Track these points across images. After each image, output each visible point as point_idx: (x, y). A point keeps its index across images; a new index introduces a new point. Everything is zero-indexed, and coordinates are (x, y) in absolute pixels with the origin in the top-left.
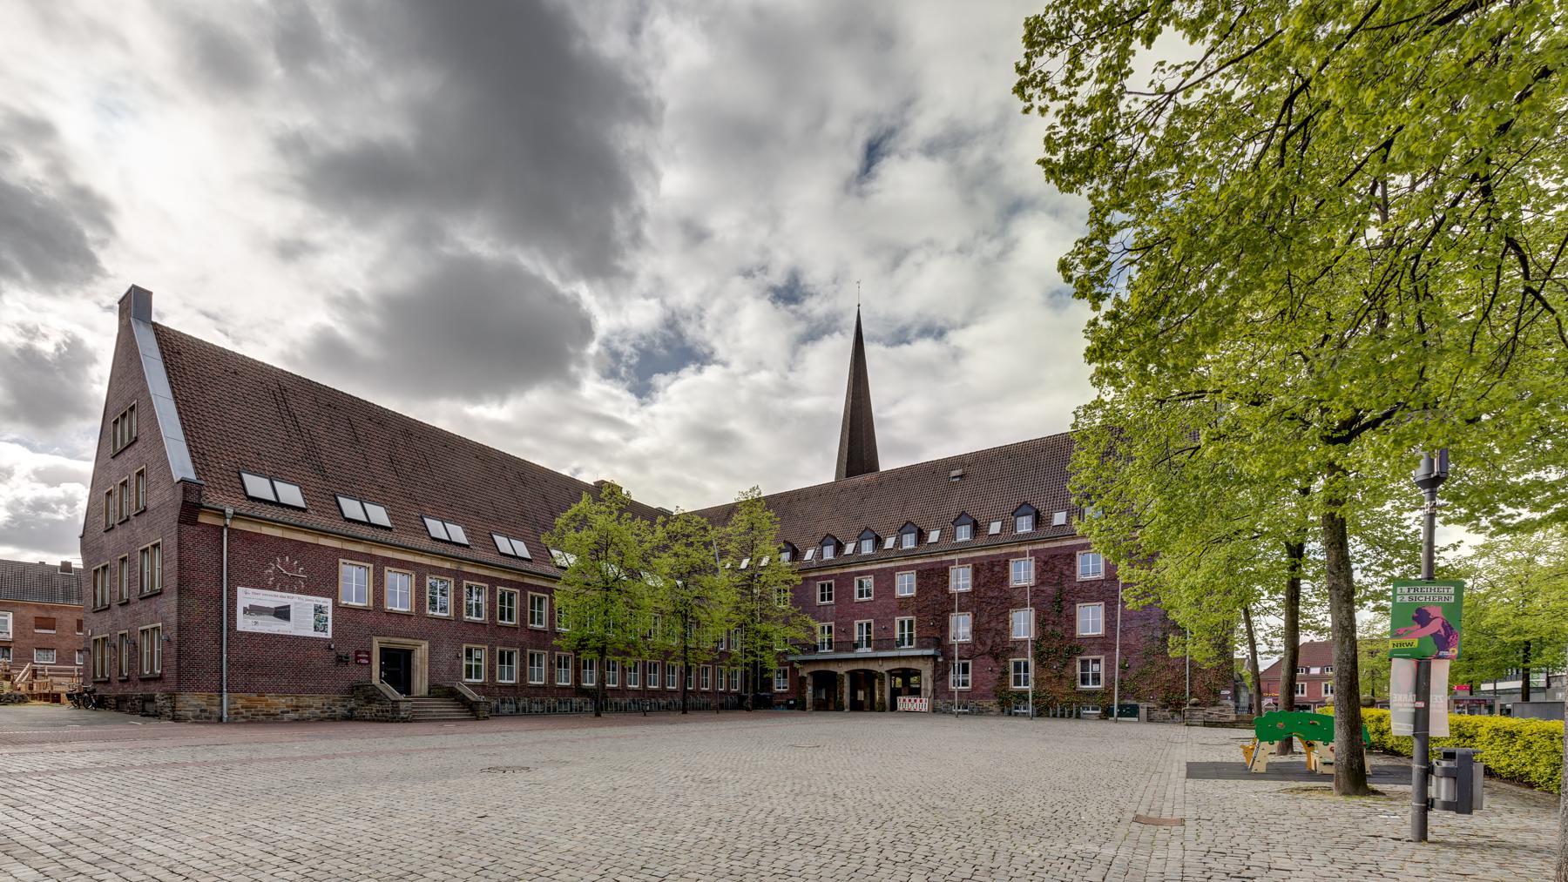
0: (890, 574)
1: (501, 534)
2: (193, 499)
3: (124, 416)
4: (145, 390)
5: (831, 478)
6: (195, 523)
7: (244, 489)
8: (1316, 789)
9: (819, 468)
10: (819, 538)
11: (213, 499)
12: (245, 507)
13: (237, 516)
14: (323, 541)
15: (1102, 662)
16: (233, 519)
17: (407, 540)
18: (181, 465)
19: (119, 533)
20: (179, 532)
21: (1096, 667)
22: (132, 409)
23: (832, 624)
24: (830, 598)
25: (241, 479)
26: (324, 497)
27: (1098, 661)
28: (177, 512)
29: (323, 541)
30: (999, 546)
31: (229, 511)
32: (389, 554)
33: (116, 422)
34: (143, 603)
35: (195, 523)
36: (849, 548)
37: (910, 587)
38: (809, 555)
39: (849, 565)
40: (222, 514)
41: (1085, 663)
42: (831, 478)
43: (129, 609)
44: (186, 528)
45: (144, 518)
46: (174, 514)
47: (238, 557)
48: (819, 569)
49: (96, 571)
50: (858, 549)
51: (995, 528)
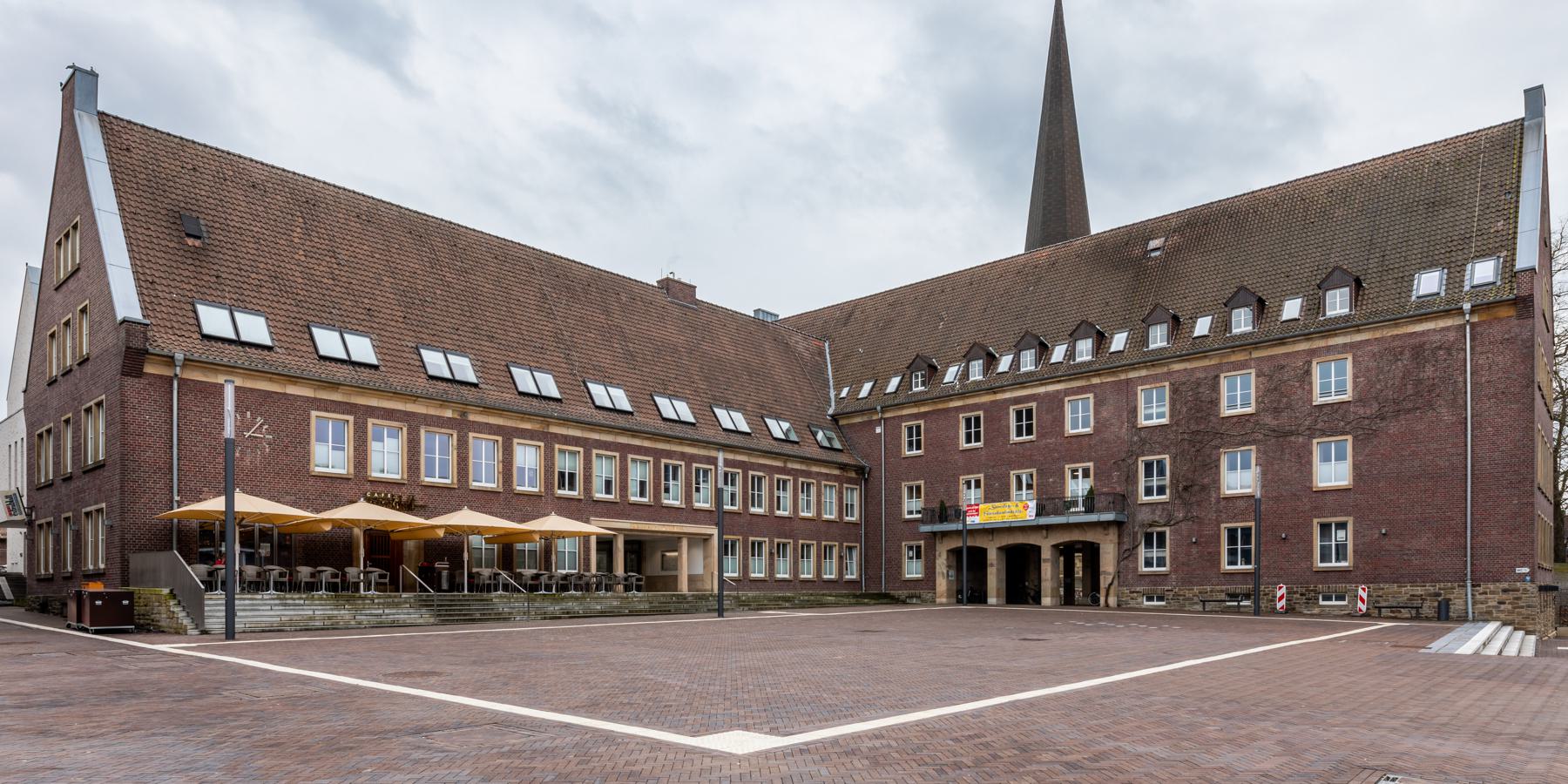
0: (1128, 389)
1: (521, 366)
2: (137, 343)
3: (67, 236)
4: (88, 202)
5: (1022, 251)
6: (139, 374)
7: (199, 326)
8: (259, 645)
9: (1001, 234)
10: (1013, 340)
11: (163, 341)
12: (200, 351)
13: (188, 362)
14: (292, 390)
15: (1350, 527)
16: (184, 366)
17: (396, 382)
18: (127, 302)
19: (63, 386)
20: (122, 386)
21: (1341, 534)
22: (75, 227)
23: (981, 476)
24: (1029, 432)
25: (195, 311)
26: (295, 328)
27: (1342, 526)
28: (120, 361)
29: (292, 390)
30: (1204, 354)
31: (179, 356)
32: (374, 402)
33: (59, 244)
34: (87, 478)
35: (139, 374)
36: (1004, 364)
37: (1245, 397)
38: (951, 374)
39: (1002, 389)
40: (170, 360)
41: (1325, 528)
42: (1022, 251)
43: (73, 485)
44: (130, 381)
45: (89, 366)
46: (117, 363)
47: (191, 416)
48: (961, 395)
49: (40, 436)
50: (1016, 364)
51: (1203, 326)
